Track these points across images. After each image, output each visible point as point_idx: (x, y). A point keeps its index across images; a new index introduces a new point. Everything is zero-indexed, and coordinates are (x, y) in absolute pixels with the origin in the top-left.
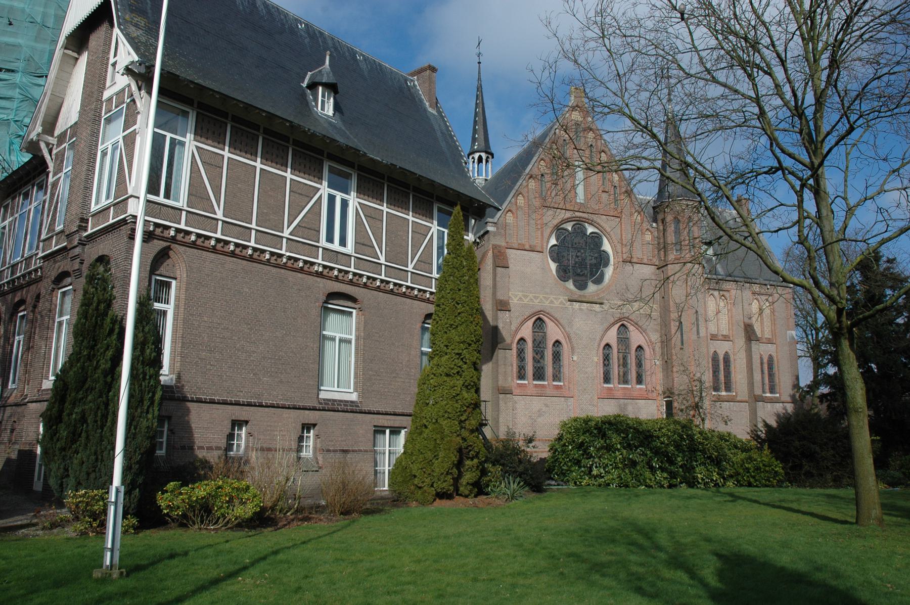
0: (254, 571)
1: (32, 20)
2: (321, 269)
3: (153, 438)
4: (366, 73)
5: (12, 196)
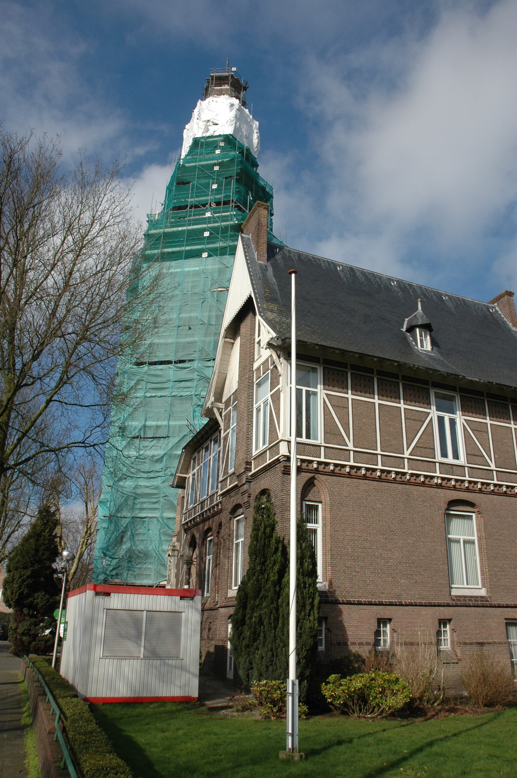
0: (414, 762)
1: (202, 323)
2: (440, 481)
3: (315, 637)
4: (453, 310)
5: (198, 450)
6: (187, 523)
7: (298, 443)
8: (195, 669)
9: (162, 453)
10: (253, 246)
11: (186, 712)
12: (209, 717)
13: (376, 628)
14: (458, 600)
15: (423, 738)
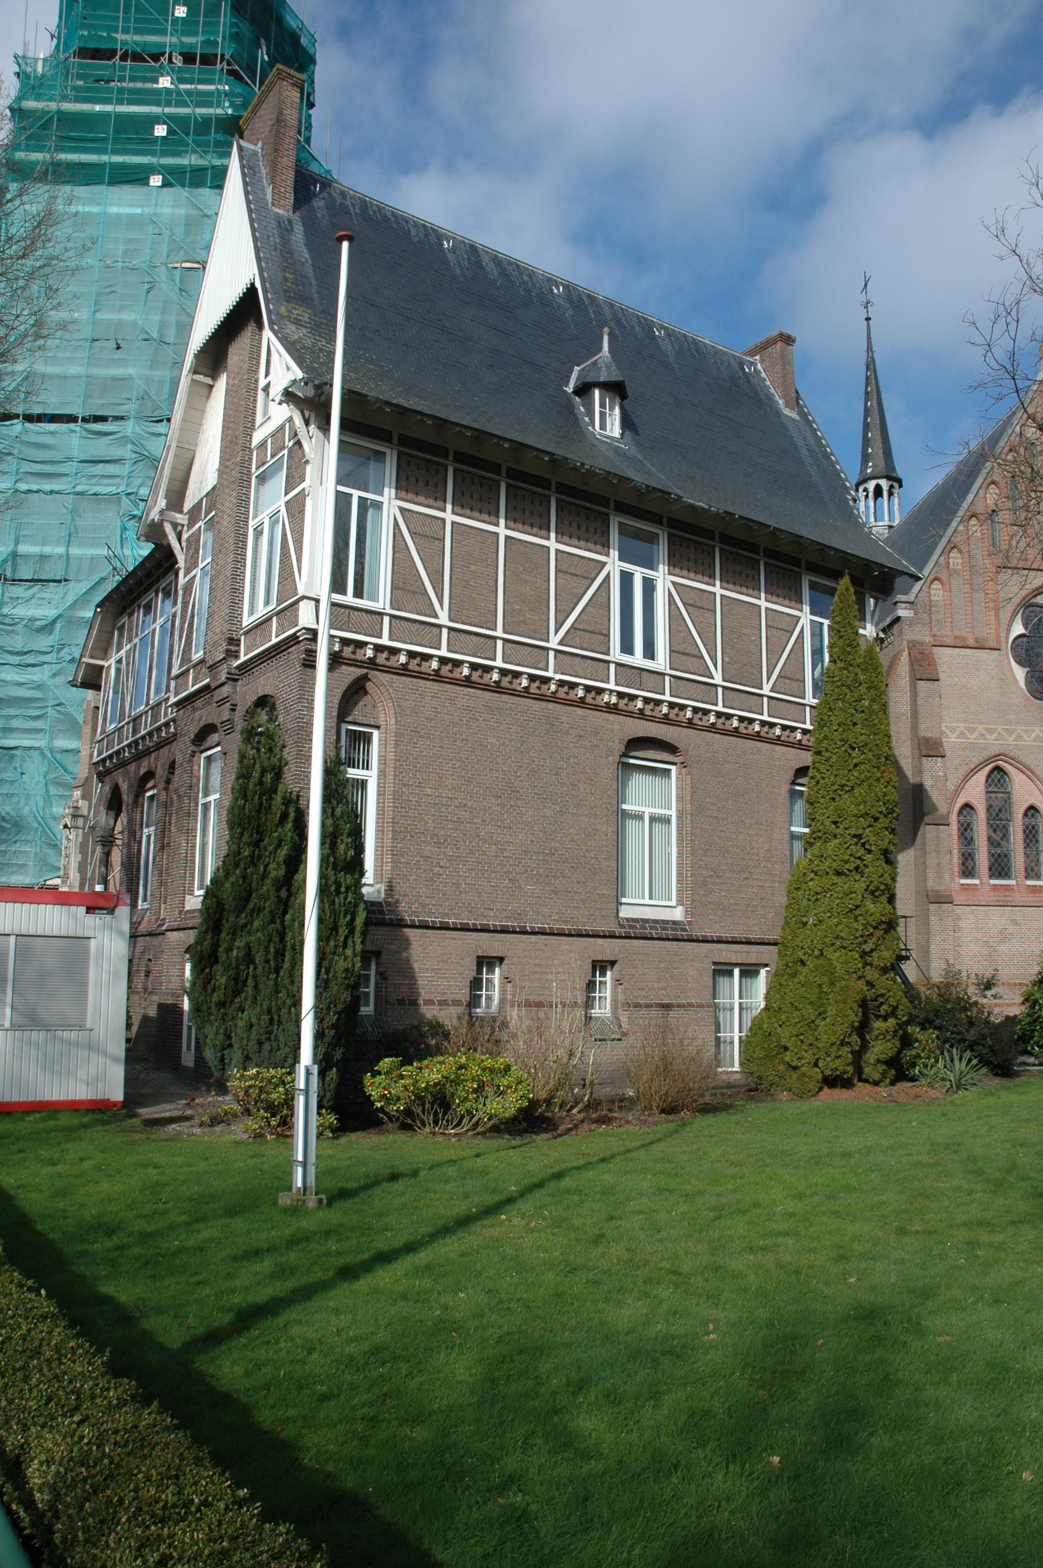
0: (526, 1206)
1: (146, 337)
2: (614, 700)
3: (354, 987)
4: (672, 359)
5: (129, 610)
6: (104, 761)
7: (334, 604)
8: (119, 1048)
9: (52, 613)
10: (264, 172)
11: (100, 1128)
12: (144, 1136)
13: (474, 974)
14: (630, 927)
15: (547, 1166)
